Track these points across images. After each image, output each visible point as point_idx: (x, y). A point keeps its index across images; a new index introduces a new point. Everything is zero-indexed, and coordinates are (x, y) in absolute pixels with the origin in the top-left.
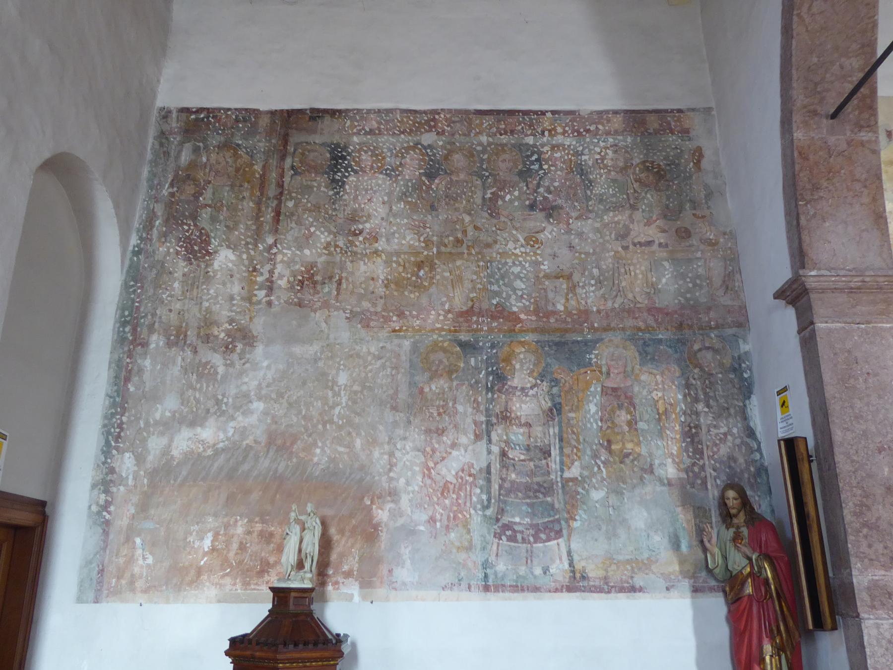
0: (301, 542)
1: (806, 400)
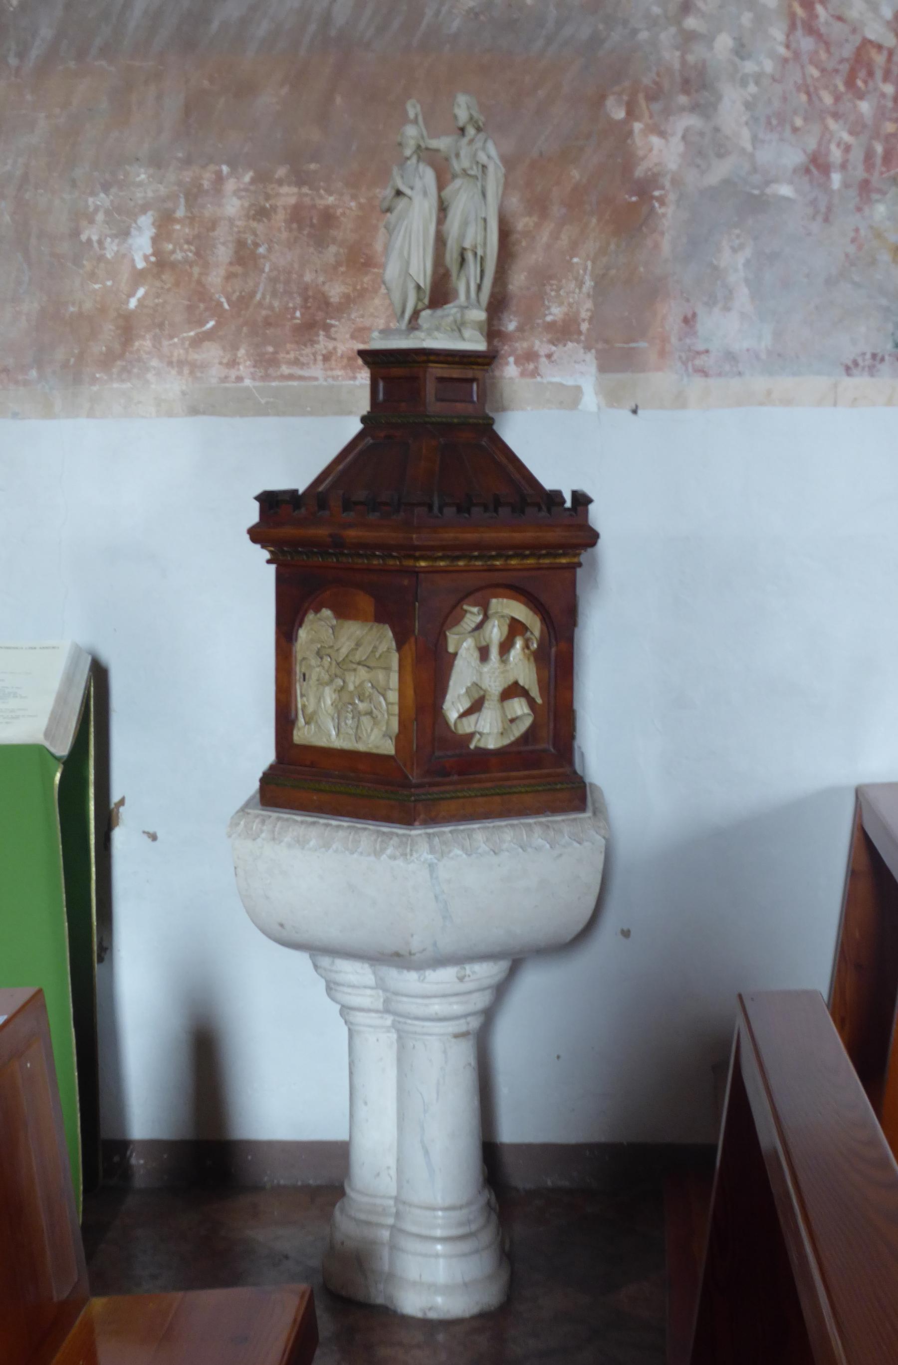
0: (443, 209)
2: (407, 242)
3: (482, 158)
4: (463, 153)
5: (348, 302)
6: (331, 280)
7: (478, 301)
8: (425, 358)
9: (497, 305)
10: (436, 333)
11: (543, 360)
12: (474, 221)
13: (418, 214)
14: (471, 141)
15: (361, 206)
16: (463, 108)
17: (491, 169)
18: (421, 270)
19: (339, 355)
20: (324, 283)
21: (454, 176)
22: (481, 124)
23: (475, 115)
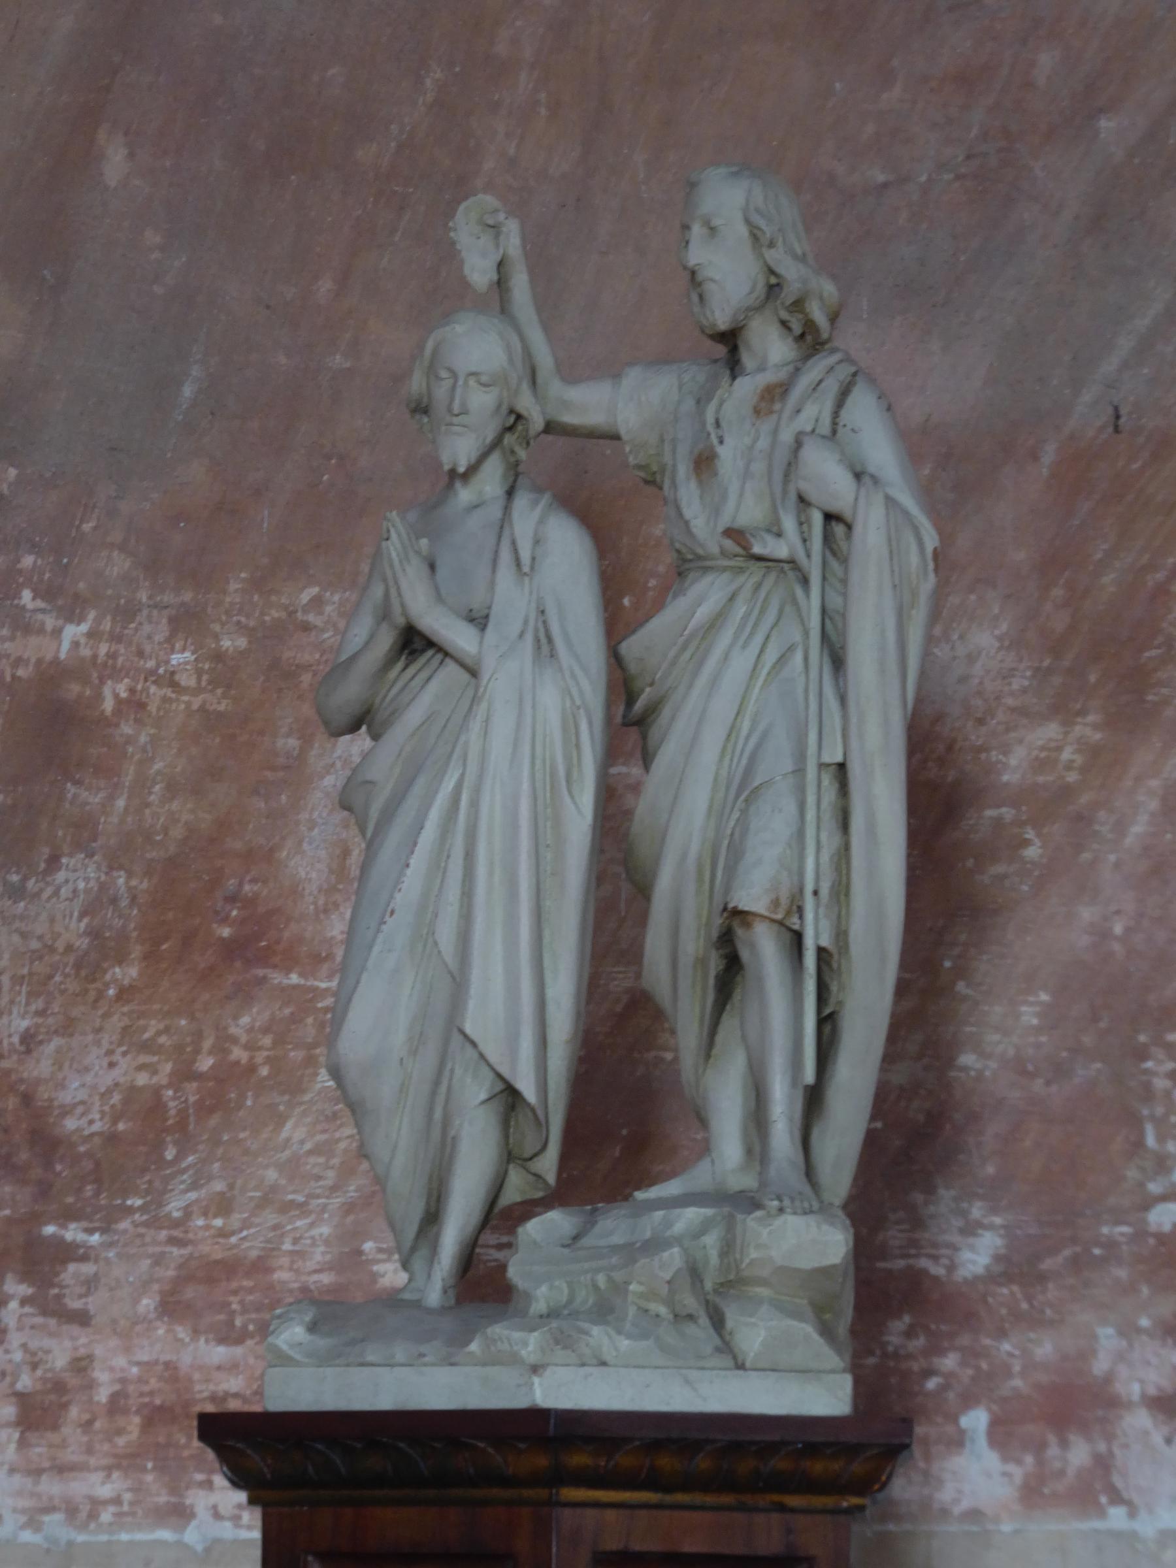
0: (632, 719)
1: (385, 1403)
2: (453, 893)
3: (827, 476)
4: (728, 456)
5: (151, 1132)
6: (68, 1027)
7: (809, 1172)
8: (542, 1461)
9: (908, 1154)
10: (598, 1336)
11: (1140, 1420)
12: (782, 779)
13: (515, 736)
14: (773, 396)
15: (222, 671)
16: (731, 238)
17: (870, 532)
18: (522, 1009)
19: (102, 1395)
20: (29, 1041)
21: (687, 565)
22: (819, 316)
23: (791, 271)
